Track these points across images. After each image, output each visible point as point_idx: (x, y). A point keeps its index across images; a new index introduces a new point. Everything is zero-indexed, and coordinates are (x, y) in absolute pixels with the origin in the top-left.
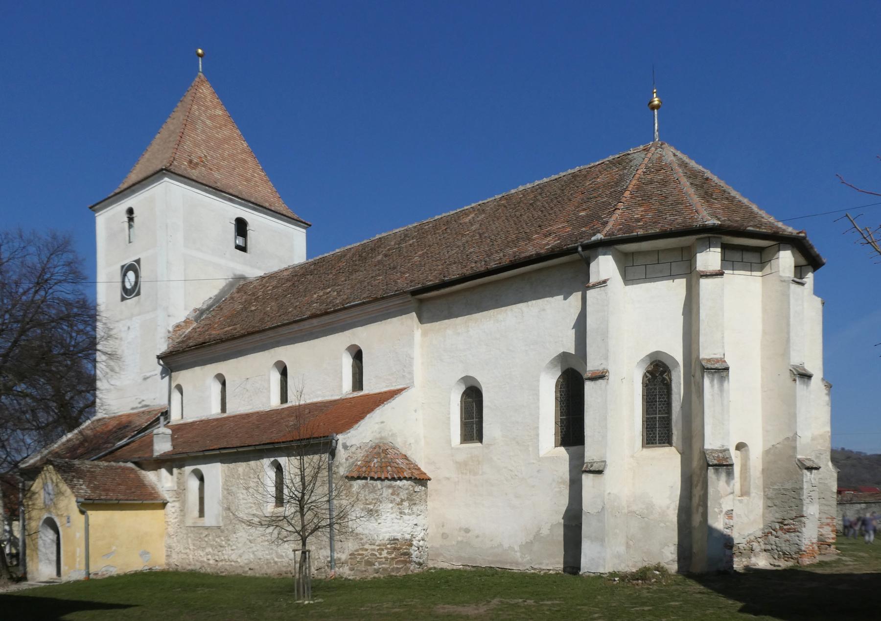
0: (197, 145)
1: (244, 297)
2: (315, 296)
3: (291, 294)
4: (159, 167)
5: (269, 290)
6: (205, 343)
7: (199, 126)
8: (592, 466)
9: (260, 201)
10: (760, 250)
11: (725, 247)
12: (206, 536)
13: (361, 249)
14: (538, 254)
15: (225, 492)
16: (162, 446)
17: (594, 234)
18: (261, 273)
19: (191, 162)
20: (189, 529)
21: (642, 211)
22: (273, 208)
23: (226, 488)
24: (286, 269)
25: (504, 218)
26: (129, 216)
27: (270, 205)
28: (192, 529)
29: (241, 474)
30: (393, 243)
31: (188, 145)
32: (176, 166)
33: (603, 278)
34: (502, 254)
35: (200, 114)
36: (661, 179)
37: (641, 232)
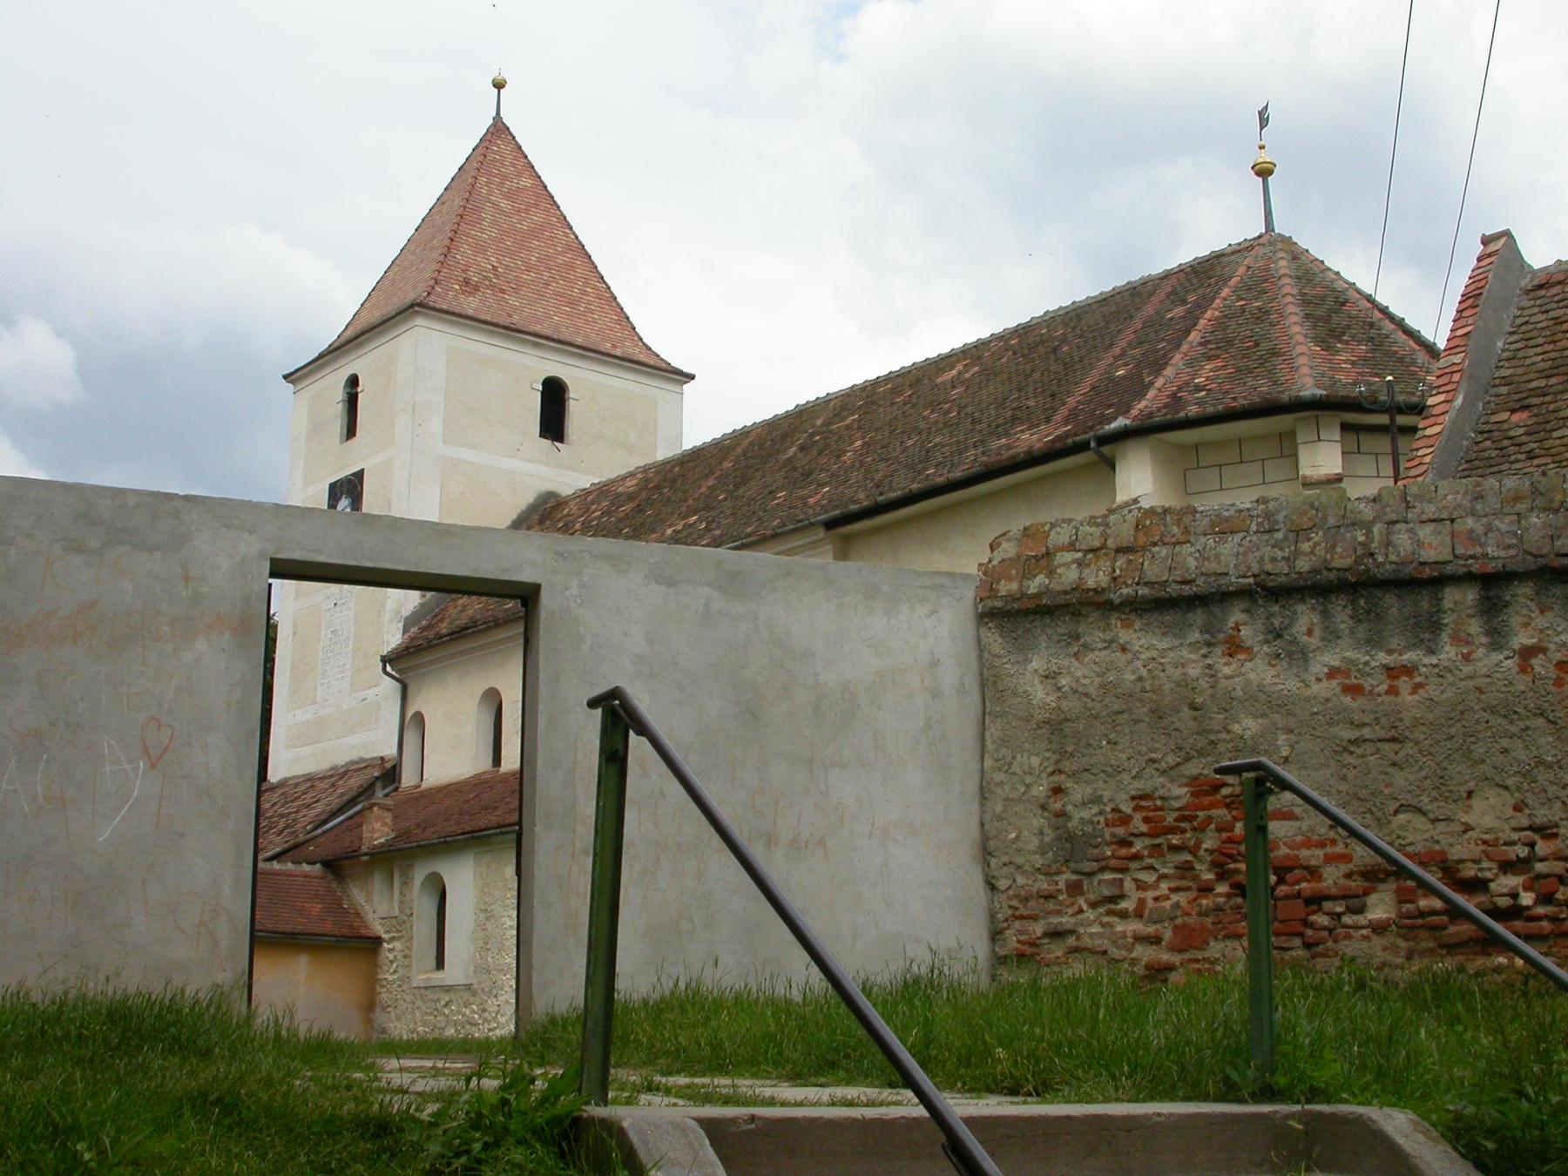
0: (480, 249)
1: (1227, 671)
2: (669, 532)
3: (630, 526)
4: (407, 301)
5: (593, 520)
6: (467, 629)
7: (487, 214)
9: (594, 340)
11: (1345, 427)
12: (446, 1005)
13: (765, 432)
15: (482, 916)
16: (378, 831)
18: (585, 481)
19: (466, 282)
20: (416, 991)
21: (1211, 370)
22: (618, 352)
23: (484, 907)
24: (631, 475)
25: (1005, 376)
26: (349, 390)
27: (614, 346)
28: (423, 991)
29: (946, 957)
30: (819, 422)
31: (464, 252)
32: (439, 295)
35: (491, 192)
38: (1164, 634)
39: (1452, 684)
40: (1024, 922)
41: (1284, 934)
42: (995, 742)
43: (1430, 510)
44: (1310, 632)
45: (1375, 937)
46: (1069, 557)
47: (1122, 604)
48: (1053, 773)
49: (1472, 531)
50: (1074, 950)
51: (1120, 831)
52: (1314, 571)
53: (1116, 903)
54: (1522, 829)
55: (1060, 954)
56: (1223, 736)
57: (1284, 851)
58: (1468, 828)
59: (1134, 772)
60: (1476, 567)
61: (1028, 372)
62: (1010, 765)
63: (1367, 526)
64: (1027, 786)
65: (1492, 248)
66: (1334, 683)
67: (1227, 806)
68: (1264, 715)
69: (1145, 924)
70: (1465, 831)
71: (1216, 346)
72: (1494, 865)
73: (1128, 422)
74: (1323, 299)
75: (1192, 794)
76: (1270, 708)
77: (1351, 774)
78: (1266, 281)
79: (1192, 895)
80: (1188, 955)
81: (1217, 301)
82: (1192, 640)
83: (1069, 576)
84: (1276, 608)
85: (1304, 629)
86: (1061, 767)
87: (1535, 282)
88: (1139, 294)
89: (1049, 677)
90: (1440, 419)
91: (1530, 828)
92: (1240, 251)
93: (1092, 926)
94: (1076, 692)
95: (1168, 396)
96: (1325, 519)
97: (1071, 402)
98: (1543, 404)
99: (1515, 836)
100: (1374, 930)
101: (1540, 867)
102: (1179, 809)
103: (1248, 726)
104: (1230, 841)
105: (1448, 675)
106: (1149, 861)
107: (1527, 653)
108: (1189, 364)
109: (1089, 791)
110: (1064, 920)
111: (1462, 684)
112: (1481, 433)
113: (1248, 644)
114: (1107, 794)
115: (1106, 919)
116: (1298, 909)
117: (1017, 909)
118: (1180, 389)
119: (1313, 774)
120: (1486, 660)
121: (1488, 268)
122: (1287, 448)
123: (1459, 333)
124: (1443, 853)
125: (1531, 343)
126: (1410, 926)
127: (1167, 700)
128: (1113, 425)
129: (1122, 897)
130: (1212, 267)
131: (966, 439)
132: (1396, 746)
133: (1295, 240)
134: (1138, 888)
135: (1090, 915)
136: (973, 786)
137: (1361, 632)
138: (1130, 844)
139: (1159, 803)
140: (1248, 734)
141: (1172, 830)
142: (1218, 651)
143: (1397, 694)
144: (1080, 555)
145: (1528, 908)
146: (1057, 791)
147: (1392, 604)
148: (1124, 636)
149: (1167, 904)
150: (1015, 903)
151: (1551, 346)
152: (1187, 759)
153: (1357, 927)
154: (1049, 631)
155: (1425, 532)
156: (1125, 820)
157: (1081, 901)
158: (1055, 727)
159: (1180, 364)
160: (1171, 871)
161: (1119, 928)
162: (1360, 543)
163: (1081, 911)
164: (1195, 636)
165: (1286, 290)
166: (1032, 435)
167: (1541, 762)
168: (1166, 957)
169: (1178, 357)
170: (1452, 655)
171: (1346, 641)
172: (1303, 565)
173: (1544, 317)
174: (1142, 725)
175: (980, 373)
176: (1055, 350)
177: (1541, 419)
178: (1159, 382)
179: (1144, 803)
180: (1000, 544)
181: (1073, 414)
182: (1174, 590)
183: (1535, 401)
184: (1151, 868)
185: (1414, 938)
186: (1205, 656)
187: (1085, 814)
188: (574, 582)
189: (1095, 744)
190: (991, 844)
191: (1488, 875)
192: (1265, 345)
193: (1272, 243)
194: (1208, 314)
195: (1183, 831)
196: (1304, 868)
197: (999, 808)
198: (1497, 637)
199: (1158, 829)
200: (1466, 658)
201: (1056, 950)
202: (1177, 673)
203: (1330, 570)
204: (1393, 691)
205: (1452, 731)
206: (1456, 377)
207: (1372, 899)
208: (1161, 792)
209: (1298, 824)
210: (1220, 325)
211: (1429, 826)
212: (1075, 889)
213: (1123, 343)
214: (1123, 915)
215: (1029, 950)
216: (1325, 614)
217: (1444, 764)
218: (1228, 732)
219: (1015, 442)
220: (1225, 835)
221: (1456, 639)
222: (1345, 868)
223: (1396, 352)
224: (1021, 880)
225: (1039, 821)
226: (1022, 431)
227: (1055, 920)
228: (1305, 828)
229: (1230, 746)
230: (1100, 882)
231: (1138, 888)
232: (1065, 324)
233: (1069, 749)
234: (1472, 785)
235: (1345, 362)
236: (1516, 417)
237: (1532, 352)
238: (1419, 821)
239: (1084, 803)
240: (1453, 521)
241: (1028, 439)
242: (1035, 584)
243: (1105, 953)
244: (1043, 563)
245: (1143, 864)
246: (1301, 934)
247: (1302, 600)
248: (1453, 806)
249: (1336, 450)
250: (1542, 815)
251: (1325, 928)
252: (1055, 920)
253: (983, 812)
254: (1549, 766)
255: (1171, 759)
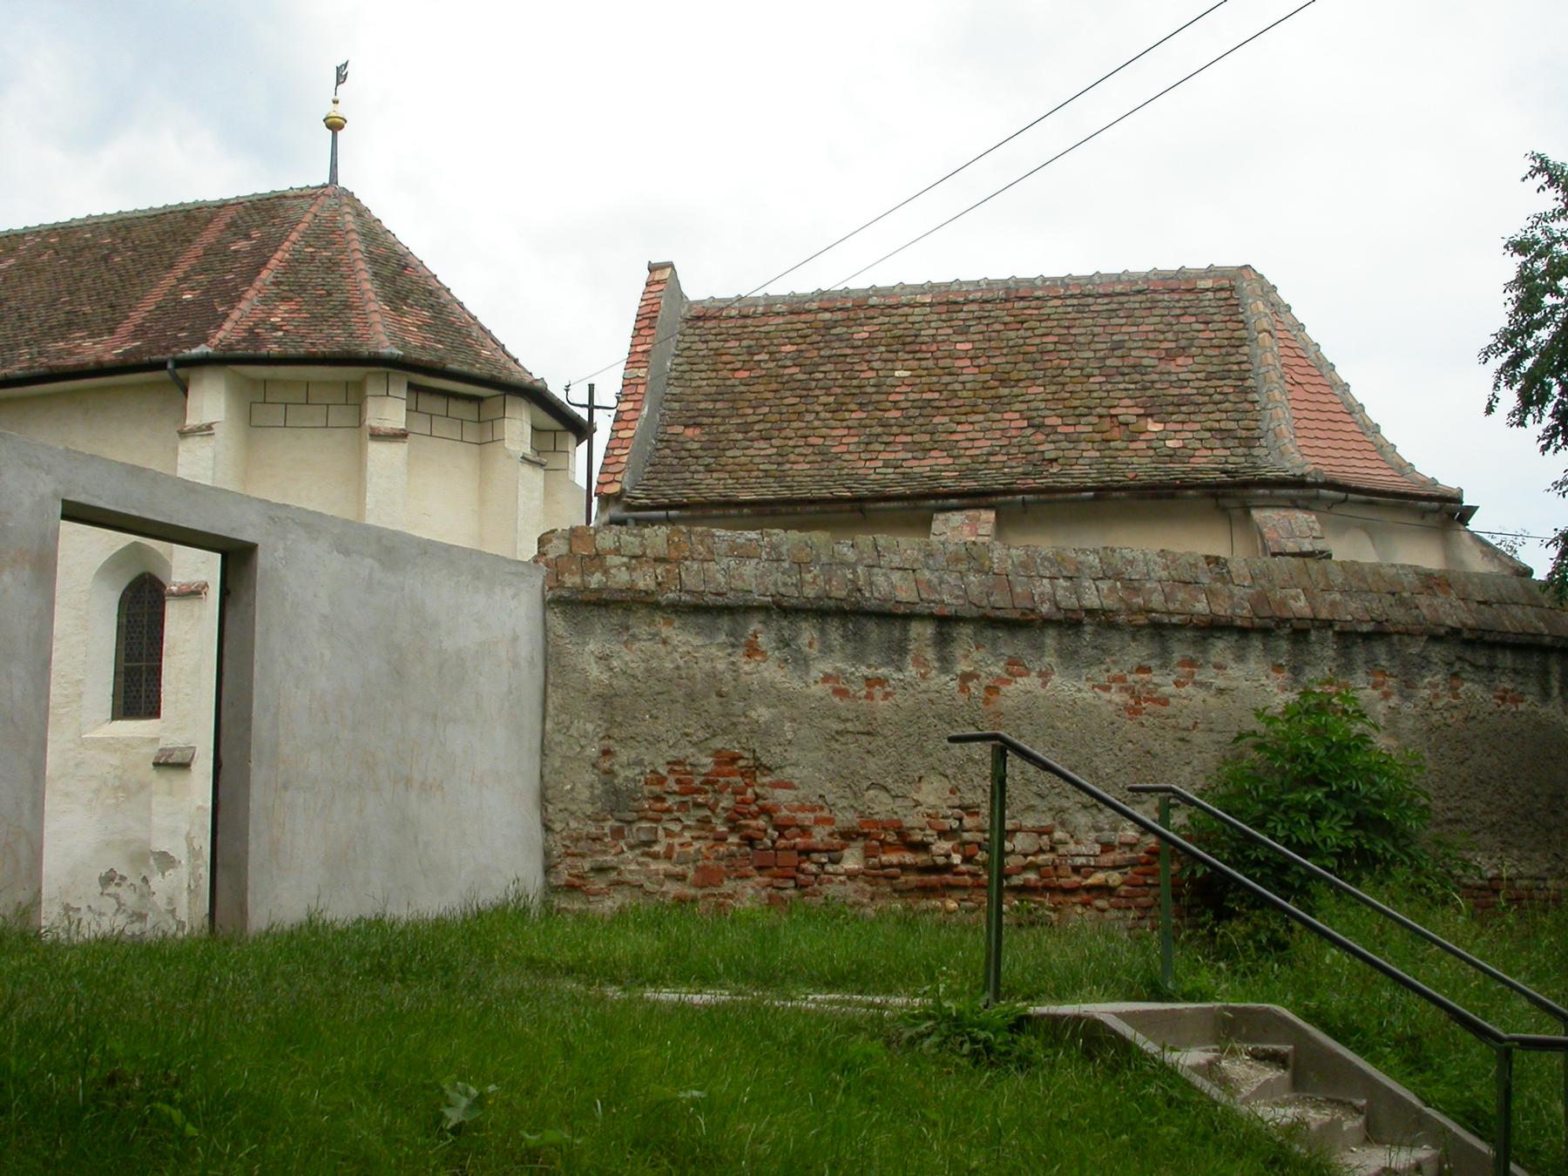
1: (746, 668)
8: (170, 756)
10: (478, 400)
11: (412, 387)
14: (99, 363)
17: (196, 345)
21: (286, 312)
25: (49, 275)
33: (207, 420)
34: (35, 350)
36: (327, 257)
37: (274, 349)
38: (697, 634)
39: (913, 695)
40: (574, 859)
41: (782, 877)
42: (556, 708)
43: (897, 561)
44: (810, 645)
45: (848, 882)
46: (617, 560)
47: (668, 606)
48: (603, 738)
49: (929, 581)
50: (618, 883)
51: (657, 789)
52: (819, 598)
53: (650, 847)
54: (954, 807)
55: (603, 886)
56: (742, 719)
57: (785, 812)
58: (918, 804)
59: (671, 743)
60: (936, 610)
61: (77, 276)
62: (568, 729)
63: (852, 566)
64: (582, 747)
65: (658, 276)
66: (827, 685)
67: (742, 775)
68: (775, 706)
69: (674, 865)
70: (916, 806)
71: (290, 286)
72: (935, 833)
73: (210, 350)
74: (387, 260)
75: (716, 763)
76: (779, 700)
77: (837, 757)
78: (333, 232)
79: (711, 843)
80: (707, 891)
81: (287, 243)
82: (720, 641)
83: (622, 577)
84: (785, 623)
85: (807, 641)
86: (610, 733)
87: (693, 313)
88: (195, 219)
89: (604, 658)
90: (631, 425)
91: (959, 807)
92: (302, 197)
93: (631, 865)
94: (625, 673)
95: (245, 330)
96: (818, 556)
97: (137, 317)
98: (713, 424)
99: (949, 812)
100: (849, 877)
101: (967, 836)
102: (705, 775)
103: (762, 713)
104: (743, 802)
105: (910, 688)
106: (678, 814)
107: (966, 678)
108: (264, 301)
109: (633, 755)
110: (608, 858)
111: (920, 696)
112: (661, 441)
113: (764, 648)
114: (647, 759)
115: (641, 859)
116: (793, 858)
117: (568, 847)
118: (256, 325)
119: (809, 755)
120: (938, 680)
121: (659, 294)
122: (355, 399)
123: (639, 349)
124: (899, 821)
125: (695, 367)
126: (875, 875)
127: (699, 686)
128: (194, 351)
129: (655, 842)
130: (274, 207)
131: (15, 336)
132: (870, 738)
133: (356, 196)
134: (667, 835)
135: (629, 855)
136: (536, 743)
137: (849, 649)
138: (663, 800)
139: (688, 768)
140: (762, 720)
141: (698, 791)
142: (741, 651)
143: (872, 699)
144: (625, 560)
145: (957, 865)
146: (606, 753)
147: (873, 631)
148: (666, 631)
149: (691, 850)
150: (567, 843)
151: (714, 374)
152: (714, 736)
153: (836, 874)
154: (604, 621)
155: (896, 577)
156: (661, 780)
157: (622, 843)
158: (606, 701)
159: (255, 300)
160: (693, 823)
161: (653, 867)
162: (850, 580)
163: (622, 852)
164: (722, 638)
165: (356, 245)
166: (95, 344)
167: (971, 759)
168: (692, 892)
169: (251, 293)
170: (914, 673)
171: (838, 655)
172: (810, 592)
173: (705, 346)
174: (678, 705)
175: (18, 267)
176: (106, 258)
177: (712, 437)
178: (235, 315)
179: (677, 768)
180: (551, 541)
181: (140, 331)
182: (710, 599)
183: (705, 420)
184: (678, 820)
185: (877, 884)
186: (730, 655)
187: (629, 773)
188: (281, 546)
189: (639, 716)
190: (550, 793)
191: (931, 839)
192: (337, 296)
193: (333, 196)
194: (279, 255)
195: (706, 792)
196: (798, 826)
197: (557, 764)
198: (946, 663)
199: (687, 789)
200: (924, 676)
201: (599, 883)
202: (708, 666)
203: (830, 598)
204: (869, 696)
205: (911, 730)
206: (641, 389)
207: (846, 852)
208: (692, 760)
209: (795, 793)
210: (291, 266)
211: (891, 801)
212: (617, 833)
213: (186, 267)
214: (655, 856)
215: (577, 882)
216: (823, 632)
217: (904, 755)
218: (746, 717)
219: (76, 347)
220: (739, 798)
221: (916, 662)
222: (828, 829)
223: (454, 323)
224: (573, 824)
225: (590, 777)
226: (81, 338)
227: (601, 858)
228: (800, 796)
229: (747, 728)
230: (638, 830)
231: (667, 835)
232: (113, 234)
233: (619, 719)
234: (922, 771)
235: (413, 325)
236: (689, 432)
237: (697, 375)
238: (883, 796)
239: (629, 764)
240: (914, 571)
241: (92, 349)
242: (595, 580)
243: (641, 886)
244: (597, 562)
245: (672, 816)
246: (794, 878)
247: (806, 619)
248: (908, 787)
249: (402, 405)
250: (969, 798)
251: (813, 874)
252: (601, 858)
253: (542, 766)
254: (976, 762)
255: (701, 734)
